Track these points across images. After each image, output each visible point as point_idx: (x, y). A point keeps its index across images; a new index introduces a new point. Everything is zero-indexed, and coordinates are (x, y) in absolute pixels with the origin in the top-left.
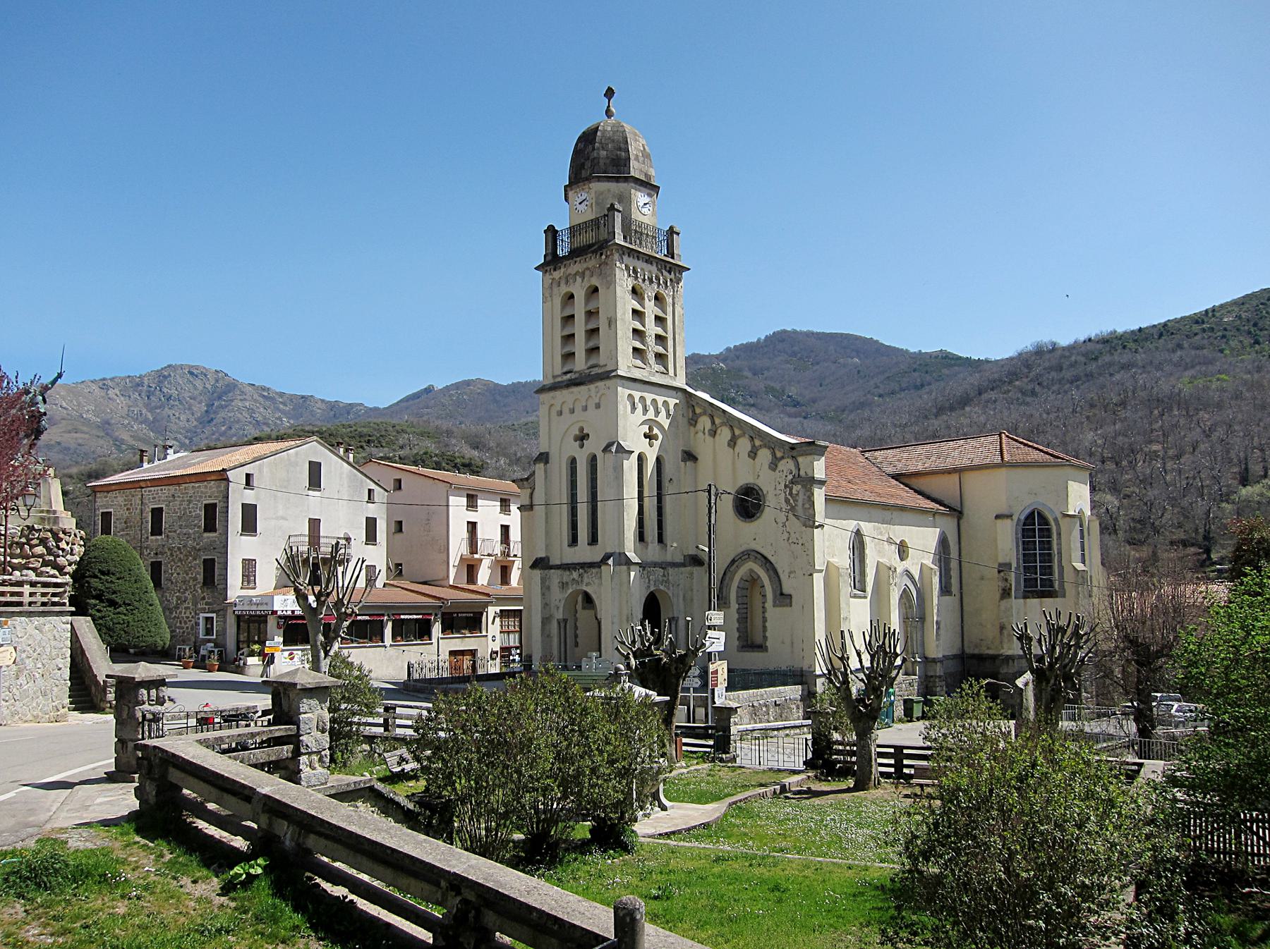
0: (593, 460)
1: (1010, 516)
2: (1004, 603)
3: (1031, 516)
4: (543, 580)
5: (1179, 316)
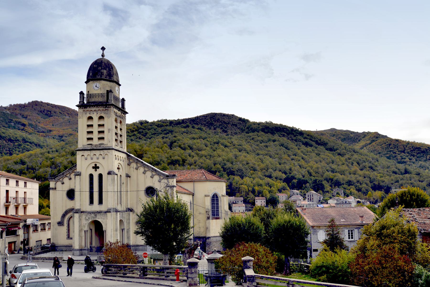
0: (100, 176)
1: (209, 196)
2: (208, 221)
3: (214, 195)
4: (79, 217)
5: (187, 118)
